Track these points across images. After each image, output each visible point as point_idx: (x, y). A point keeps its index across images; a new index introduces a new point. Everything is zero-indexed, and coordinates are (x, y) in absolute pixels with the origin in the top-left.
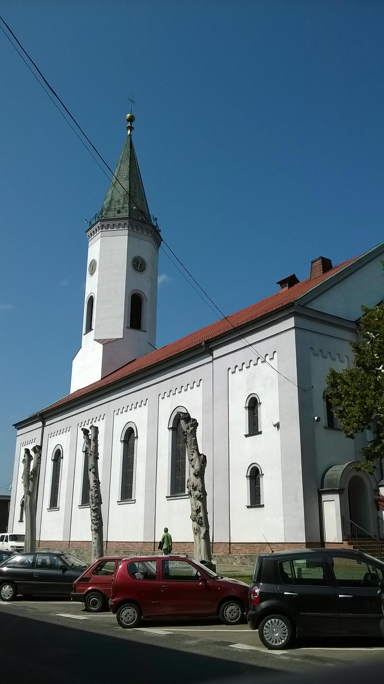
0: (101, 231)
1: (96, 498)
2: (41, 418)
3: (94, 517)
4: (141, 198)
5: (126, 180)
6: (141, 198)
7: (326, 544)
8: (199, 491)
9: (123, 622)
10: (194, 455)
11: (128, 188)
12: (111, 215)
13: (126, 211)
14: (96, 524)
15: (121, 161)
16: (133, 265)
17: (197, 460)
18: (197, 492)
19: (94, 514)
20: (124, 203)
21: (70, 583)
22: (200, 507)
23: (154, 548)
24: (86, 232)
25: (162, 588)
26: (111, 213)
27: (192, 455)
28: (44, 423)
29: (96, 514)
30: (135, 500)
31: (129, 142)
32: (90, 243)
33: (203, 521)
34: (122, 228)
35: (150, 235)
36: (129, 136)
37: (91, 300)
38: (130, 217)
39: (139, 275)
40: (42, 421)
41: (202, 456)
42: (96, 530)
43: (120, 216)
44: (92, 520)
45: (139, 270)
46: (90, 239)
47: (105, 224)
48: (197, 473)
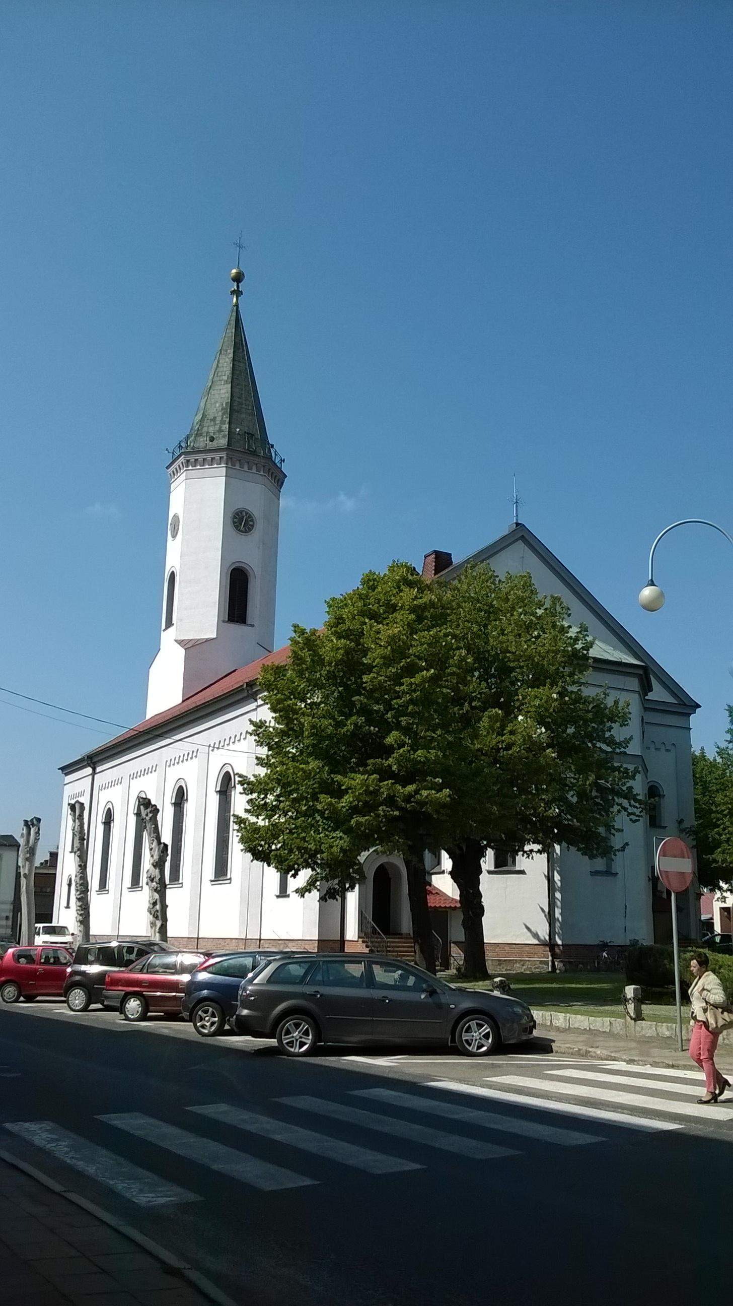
0: (186, 470)
1: (81, 885)
2: (89, 762)
3: (79, 906)
5: (227, 384)
7: (346, 942)
8: (156, 883)
9: (5, 998)
10: (154, 843)
12: (202, 442)
13: (224, 436)
14: (81, 915)
15: (221, 350)
16: (234, 522)
17: (157, 850)
18: (155, 883)
20: (222, 422)
23: (197, 945)
24: (168, 468)
26: (201, 440)
27: (152, 844)
28: (94, 769)
30: (182, 883)
31: (234, 318)
32: (173, 486)
33: (159, 914)
36: (234, 306)
37: (173, 576)
39: (243, 538)
40: (92, 766)
42: (81, 922)
43: (215, 444)
44: (77, 910)
45: (243, 530)
46: (173, 480)
47: (192, 458)
48: (155, 864)
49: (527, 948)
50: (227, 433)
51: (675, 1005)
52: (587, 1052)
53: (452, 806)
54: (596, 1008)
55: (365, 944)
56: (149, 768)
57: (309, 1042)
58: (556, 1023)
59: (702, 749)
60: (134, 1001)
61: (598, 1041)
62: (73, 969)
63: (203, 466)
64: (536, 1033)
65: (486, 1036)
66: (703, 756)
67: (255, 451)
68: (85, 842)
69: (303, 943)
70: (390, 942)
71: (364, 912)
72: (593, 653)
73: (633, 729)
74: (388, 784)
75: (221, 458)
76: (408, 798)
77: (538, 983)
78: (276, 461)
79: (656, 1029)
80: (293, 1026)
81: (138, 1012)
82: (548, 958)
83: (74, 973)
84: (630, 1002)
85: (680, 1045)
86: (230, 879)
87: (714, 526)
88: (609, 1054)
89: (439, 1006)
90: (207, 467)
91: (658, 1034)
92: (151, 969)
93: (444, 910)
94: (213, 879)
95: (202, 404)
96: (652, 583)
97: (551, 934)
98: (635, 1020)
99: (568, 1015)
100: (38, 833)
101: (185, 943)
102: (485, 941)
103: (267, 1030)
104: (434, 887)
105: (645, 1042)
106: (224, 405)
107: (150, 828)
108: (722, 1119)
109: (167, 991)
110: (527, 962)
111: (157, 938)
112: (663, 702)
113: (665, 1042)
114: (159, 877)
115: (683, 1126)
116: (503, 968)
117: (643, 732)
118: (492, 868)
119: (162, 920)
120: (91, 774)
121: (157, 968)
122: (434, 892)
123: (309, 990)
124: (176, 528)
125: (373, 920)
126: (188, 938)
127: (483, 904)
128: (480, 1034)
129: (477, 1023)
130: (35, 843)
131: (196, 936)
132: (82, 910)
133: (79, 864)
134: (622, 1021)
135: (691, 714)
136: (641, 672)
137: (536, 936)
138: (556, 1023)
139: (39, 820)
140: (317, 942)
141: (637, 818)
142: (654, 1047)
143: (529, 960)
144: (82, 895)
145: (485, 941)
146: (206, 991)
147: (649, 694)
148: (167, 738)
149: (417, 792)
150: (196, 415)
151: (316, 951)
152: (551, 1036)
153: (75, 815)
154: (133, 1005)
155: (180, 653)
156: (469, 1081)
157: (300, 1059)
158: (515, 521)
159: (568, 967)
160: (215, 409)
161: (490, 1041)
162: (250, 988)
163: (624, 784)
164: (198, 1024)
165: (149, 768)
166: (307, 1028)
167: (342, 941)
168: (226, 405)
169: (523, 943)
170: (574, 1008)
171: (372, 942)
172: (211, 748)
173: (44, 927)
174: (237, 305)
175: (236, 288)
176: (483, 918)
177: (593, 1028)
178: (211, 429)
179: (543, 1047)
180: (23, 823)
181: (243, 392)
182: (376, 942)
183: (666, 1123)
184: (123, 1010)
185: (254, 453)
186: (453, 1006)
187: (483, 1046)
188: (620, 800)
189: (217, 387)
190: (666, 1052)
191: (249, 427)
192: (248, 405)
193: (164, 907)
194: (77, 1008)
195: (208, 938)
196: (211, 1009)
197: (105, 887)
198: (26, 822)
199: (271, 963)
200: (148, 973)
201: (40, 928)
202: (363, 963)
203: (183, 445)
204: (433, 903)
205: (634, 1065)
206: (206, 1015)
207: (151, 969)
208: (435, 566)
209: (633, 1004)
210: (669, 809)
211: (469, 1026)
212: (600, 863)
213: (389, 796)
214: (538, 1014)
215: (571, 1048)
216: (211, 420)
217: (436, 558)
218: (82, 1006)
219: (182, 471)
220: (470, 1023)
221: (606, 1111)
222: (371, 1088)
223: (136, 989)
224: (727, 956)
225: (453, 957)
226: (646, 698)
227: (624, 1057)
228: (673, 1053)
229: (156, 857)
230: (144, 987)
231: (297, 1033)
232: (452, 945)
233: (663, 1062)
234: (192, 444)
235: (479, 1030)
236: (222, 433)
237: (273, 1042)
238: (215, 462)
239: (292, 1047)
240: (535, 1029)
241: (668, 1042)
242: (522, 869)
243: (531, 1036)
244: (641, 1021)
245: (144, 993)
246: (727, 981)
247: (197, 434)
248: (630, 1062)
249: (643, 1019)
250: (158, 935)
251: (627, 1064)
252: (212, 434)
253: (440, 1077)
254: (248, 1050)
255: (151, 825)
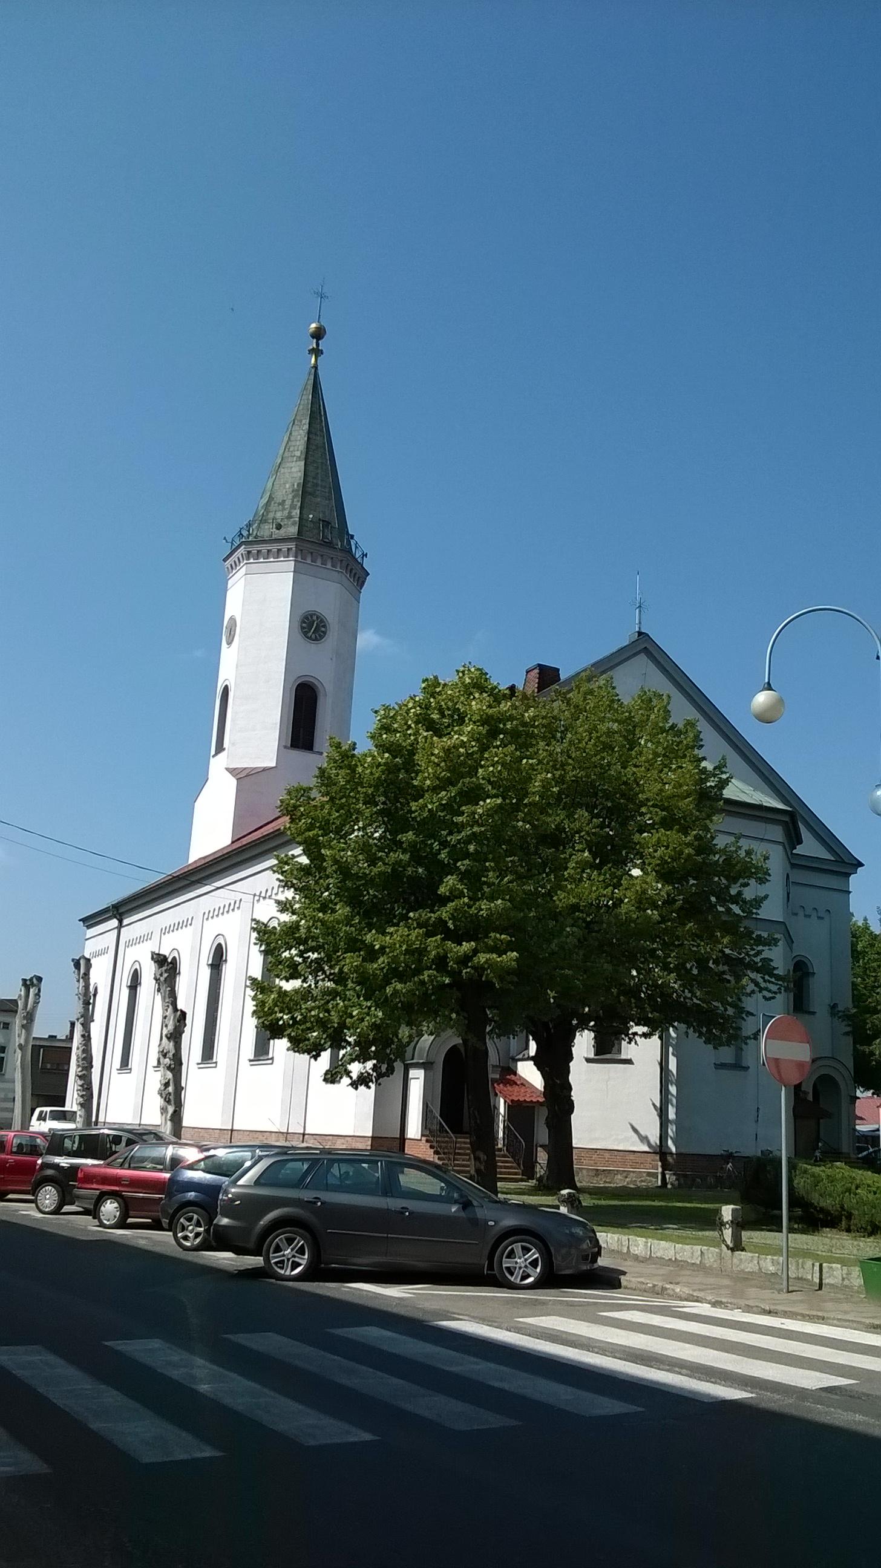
0: (246, 563)
1: (83, 1059)
3: (80, 1086)
4: (327, 494)
6: (327, 494)
7: (407, 1141)
8: (170, 1058)
10: (169, 1010)
11: (300, 477)
12: (267, 530)
13: (294, 524)
14: (82, 1096)
16: (303, 628)
17: (172, 1018)
18: (167, 1060)
19: (80, 1082)
20: (293, 507)
21: (386, 1235)
22: (169, 1080)
24: (225, 560)
25: (8, 1163)
26: (266, 527)
27: (167, 1010)
28: (120, 921)
29: (82, 1082)
31: (311, 382)
32: (230, 583)
33: (172, 1097)
34: (284, 557)
35: (338, 569)
36: (312, 367)
37: (226, 691)
38: (300, 537)
39: (313, 647)
41: (179, 1013)
43: (282, 533)
45: (313, 636)
46: (231, 575)
47: (254, 549)
48: (169, 1036)
49: (632, 1157)
50: (297, 519)
51: (781, 1231)
52: (664, 1289)
53: (520, 972)
54: (694, 1233)
55: (429, 1144)
56: (183, 921)
57: (304, 1262)
58: (635, 1251)
59: (865, 919)
60: (111, 1203)
61: (683, 1275)
62: (45, 1160)
63: (267, 559)
64: (602, 1262)
65: (534, 1264)
66: (867, 927)
67: (331, 543)
68: (91, 1007)
69: (354, 1141)
70: (461, 1142)
71: (429, 1105)
72: (729, 793)
73: (774, 888)
74: (436, 940)
75: (288, 549)
76: (465, 960)
77: (634, 1200)
78: (357, 556)
79: (758, 1263)
80: (284, 1240)
81: (115, 1217)
82: (657, 1169)
83: (45, 1166)
84: (727, 1226)
85: (785, 1283)
86: (272, 1059)
87: (859, 621)
88: (691, 1293)
89: (475, 1222)
90: (272, 560)
91: (760, 1269)
92: (131, 1162)
93: (531, 1105)
94: (252, 1058)
95: (270, 485)
96: (769, 687)
97: (663, 1137)
98: (732, 1250)
99: (650, 1240)
100: (38, 995)
101: (217, 1136)
102: (574, 1145)
103: (251, 1245)
104: (520, 1076)
105: (745, 1278)
106: (296, 486)
107: (165, 992)
108: (810, 1388)
109: (154, 1192)
110: (632, 1174)
111: (167, 1129)
112: (817, 858)
113: (768, 1280)
114: (174, 1051)
115: (753, 1395)
116: (601, 1179)
117: (788, 894)
118: (592, 1056)
119: (175, 1104)
120: (117, 927)
121: (146, 1163)
122: (518, 1083)
123: (307, 1195)
124: (232, 633)
125: (441, 1116)
126: (220, 1129)
127: (573, 1098)
128: (526, 1260)
129: (522, 1247)
130: (34, 1007)
131: (230, 1128)
132: (83, 1091)
133: (82, 1033)
134: (717, 1250)
135: (850, 874)
136: (786, 819)
137: (644, 1139)
138: (635, 1250)
139: (40, 979)
140: (370, 1139)
141: (773, 995)
142: (752, 1286)
143: (633, 1172)
144: (84, 1072)
145: (575, 1143)
146: (193, 1193)
147: (798, 847)
148: (207, 885)
149: (475, 952)
150: (261, 498)
151: (369, 1148)
152: (624, 1266)
153: (79, 974)
154: (110, 1208)
155: (231, 784)
156: (495, 1322)
157: (290, 1284)
158: (637, 630)
159: (682, 1181)
160: (284, 491)
161: (538, 1270)
162: (233, 1190)
163: (759, 953)
164: (179, 1235)
165: (183, 921)
166: (303, 1245)
167: (402, 1139)
168: (298, 485)
169: (627, 1149)
170: (667, 1232)
171: (437, 1142)
172: (257, 898)
173: (51, 1111)
174: (316, 367)
175: (315, 346)
176: (572, 1116)
177: (680, 1259)
178: (279, 515)
179: (609, 1280)
180: (21, 983)
181: (319, 471)
182: (443, 1142)
183: (732, 1390)
184: (97, 1213)
185: (330, 545)
186: (493, 1223)
187: (529, 1276)
188: (753, 975)
189: (288, 465)
190: (767, 1294)
191: (324, 513)
192: (325, 487)
193: (179, 1089)
194: (47, 1210)
195: (213, 1129)
196: (195, 1217)
197: (127, 1065)
198: (24, 980)
199: (262, 1159)
200: (129, 1168)
201: (46, 1112)
202: (379, 1164)
203: (245, 533)
204: (516, 1096)
205: (721, 1308)
206: (188, 1224)
207: (131, 1162)
208: (538, 683)
209: (730, 1229)
210: (820, 991)
211: (512, 1250)
212: (726, 1054)
213: (438, 956)
214: (607, 1238)
215: (644, 1283)
216: (279, 504)
217: (539, 673)
218: (53, 1207)
219: (242, 565)
220: (513, 1246)
221: (659, 1369)
222: (361, 1325)
223: (112, 1188)
224: (870, 1173)
225: (540, 1164)
226: (794, 852)
227: (709, 1298)
228: (776, 1295)
229: (171, 1027)
230: (125, 1186)
231: (289, 1250)
232: (539, 1149)
233: (757, 1306)
234: (255, 533)
235: (524, 1255)
236: (292, 520)
237: (257, 1261)
238: (281, 554)
239: (282, 1268)
240: (600, 1256)
241: (773, 1280)
242: (629, 1057)
243: (596, 1266)
244: (740, 1252)
245: (124, 1193)
246: (865, 1205)
247: (261, 521)
248: (715, 1304)
249: (743, 1250)
250: (169, 1123)
251: (712, 1307)
252: (279, 521)
253: (458, 1314)
254: (231, 1269)
255: (166, 987)
